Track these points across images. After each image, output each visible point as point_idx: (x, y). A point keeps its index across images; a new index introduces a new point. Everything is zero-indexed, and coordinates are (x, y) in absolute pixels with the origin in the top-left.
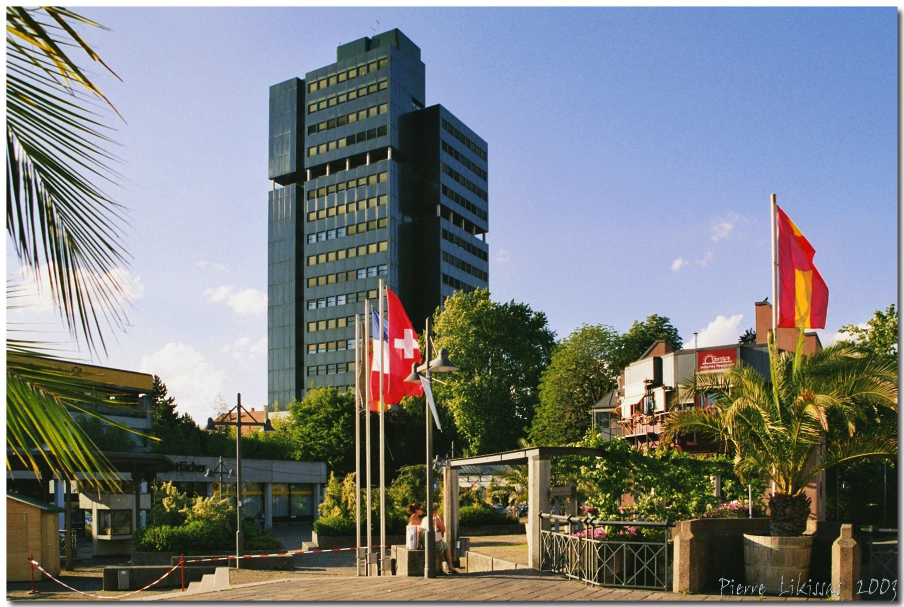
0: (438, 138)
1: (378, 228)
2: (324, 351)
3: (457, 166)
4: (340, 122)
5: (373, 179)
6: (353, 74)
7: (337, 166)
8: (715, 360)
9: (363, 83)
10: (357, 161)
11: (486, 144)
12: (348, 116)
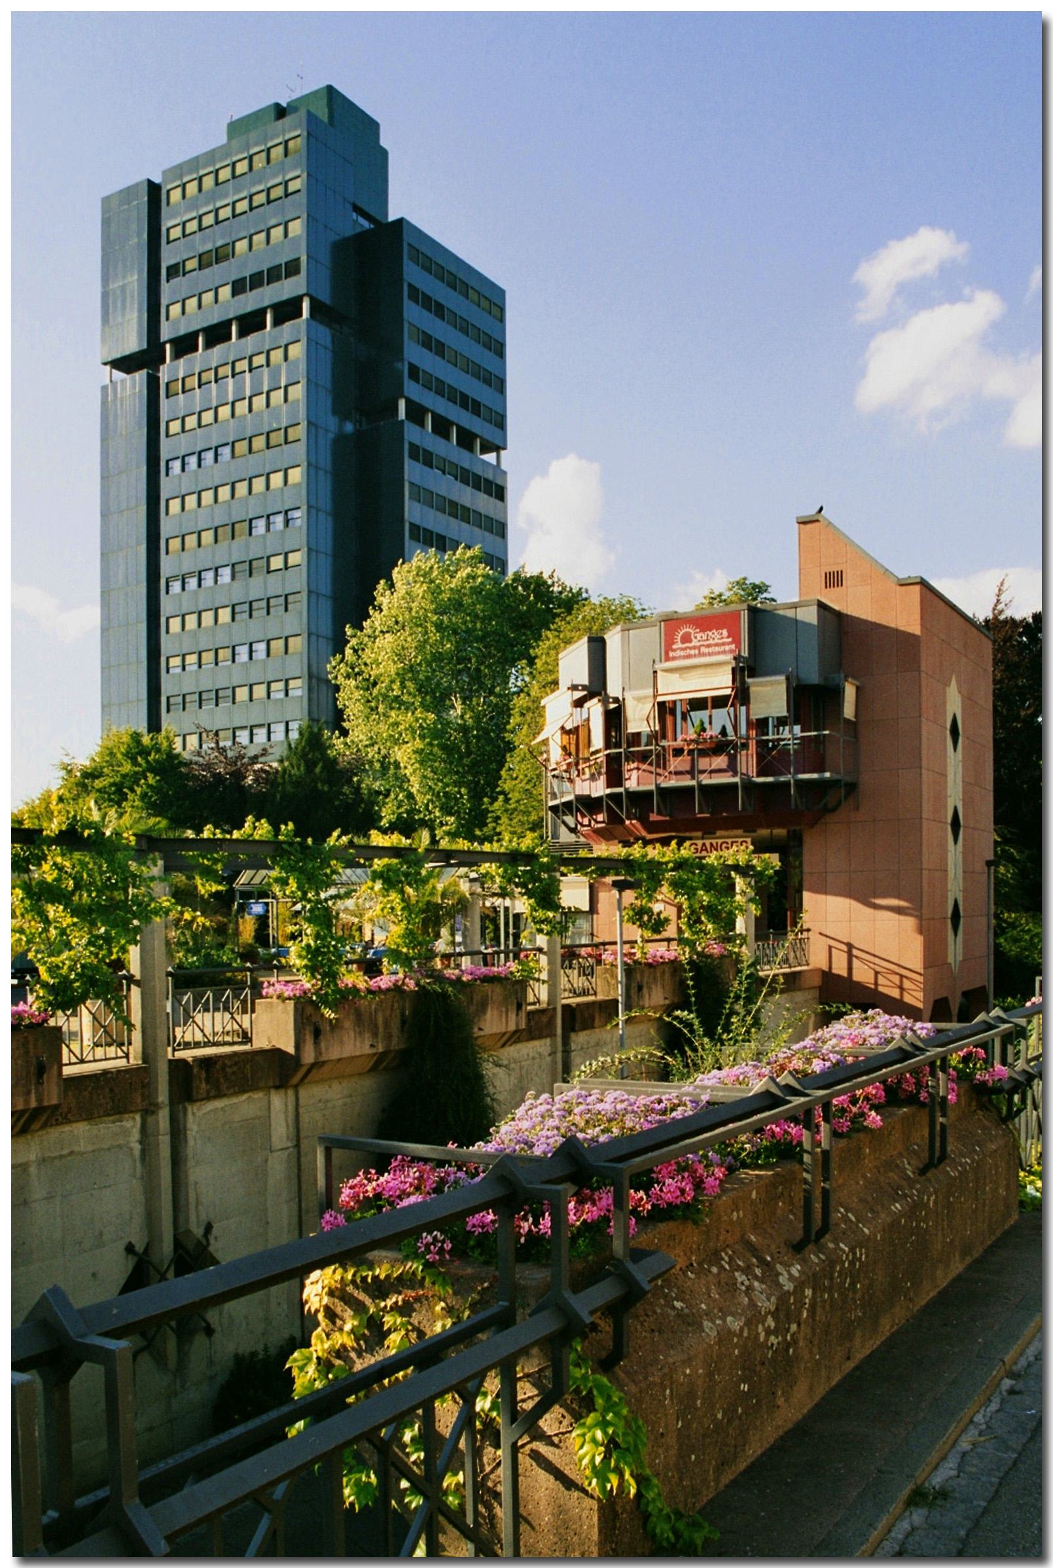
0: (399, 279)
1: (286, 442)
2: (195, 667)
3: (440, 330)
4: (221, 255)
5: (277, 356)
6: (242, 168)
7: (217, 334)
8: (698, 638)
9: (260, 182)
10: (251, 323)
11: (503, 292)
12: (234, 243)
